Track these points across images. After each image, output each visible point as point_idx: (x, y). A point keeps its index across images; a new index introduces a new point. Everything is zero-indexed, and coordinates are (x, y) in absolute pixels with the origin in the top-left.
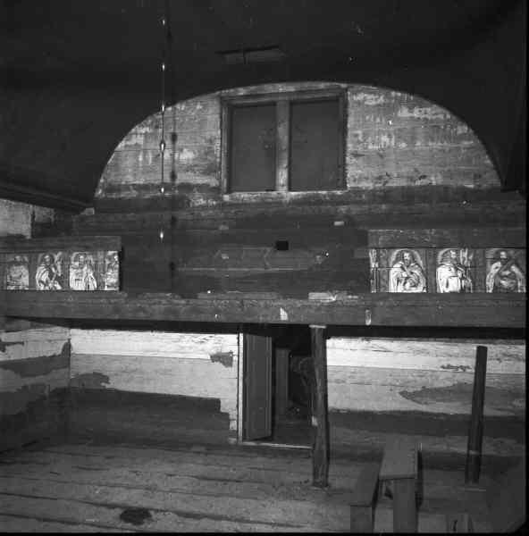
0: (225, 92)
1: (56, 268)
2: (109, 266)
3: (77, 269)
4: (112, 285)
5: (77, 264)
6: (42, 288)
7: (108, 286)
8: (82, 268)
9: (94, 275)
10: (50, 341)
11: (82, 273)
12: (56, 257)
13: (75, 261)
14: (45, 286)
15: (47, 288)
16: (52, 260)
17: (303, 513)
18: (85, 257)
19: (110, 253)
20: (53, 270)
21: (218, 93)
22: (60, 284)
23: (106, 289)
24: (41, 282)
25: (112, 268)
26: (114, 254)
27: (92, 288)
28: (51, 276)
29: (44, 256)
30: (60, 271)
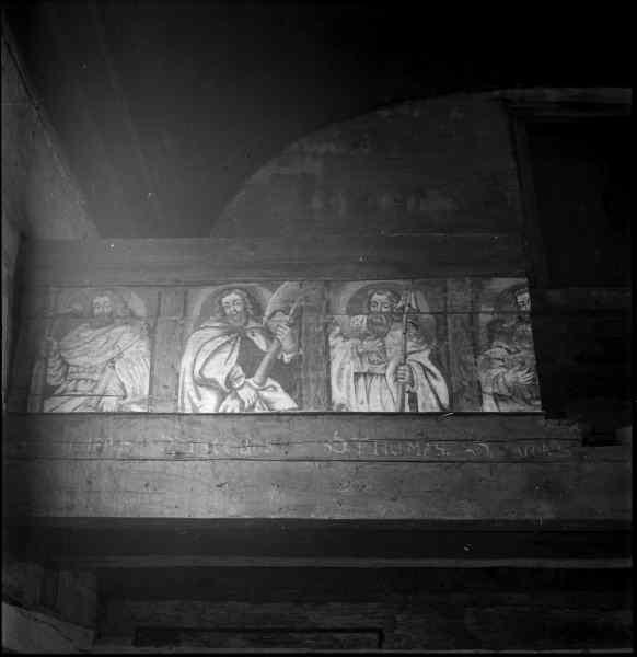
0: (510, 93)
1: (270, 335)
2: (493, 331)
3: (363, 337)
4: (514, 393)
5: (360, 321)
6: (209, 402)
7: (498, 397)
8: (382, 336)
9: (435, 358)
10: (36, 620)
11: (384, 350)
12: (272, 300)
13: (351, 312)
14: (222, 396)
15: (231, 405)
16: (255, 308)
17: (45, 634)
18: (396, 295)
19: (501, 284)
20: (260, 342)
21: (497, 93)
22: (289, 391)
23: (489, 406)
24: (203, 382)
25: (509, 336)
26: (514, 290)
27: (427, 403)
28: (249, 362)
29: (222, 294)
30: (287, 344)
